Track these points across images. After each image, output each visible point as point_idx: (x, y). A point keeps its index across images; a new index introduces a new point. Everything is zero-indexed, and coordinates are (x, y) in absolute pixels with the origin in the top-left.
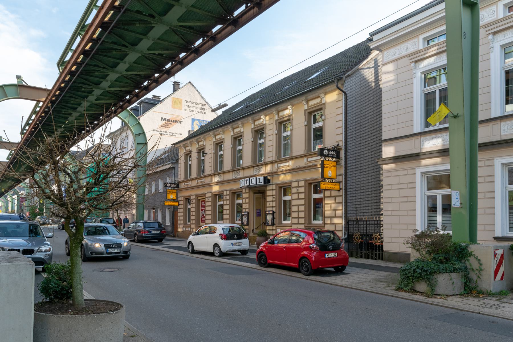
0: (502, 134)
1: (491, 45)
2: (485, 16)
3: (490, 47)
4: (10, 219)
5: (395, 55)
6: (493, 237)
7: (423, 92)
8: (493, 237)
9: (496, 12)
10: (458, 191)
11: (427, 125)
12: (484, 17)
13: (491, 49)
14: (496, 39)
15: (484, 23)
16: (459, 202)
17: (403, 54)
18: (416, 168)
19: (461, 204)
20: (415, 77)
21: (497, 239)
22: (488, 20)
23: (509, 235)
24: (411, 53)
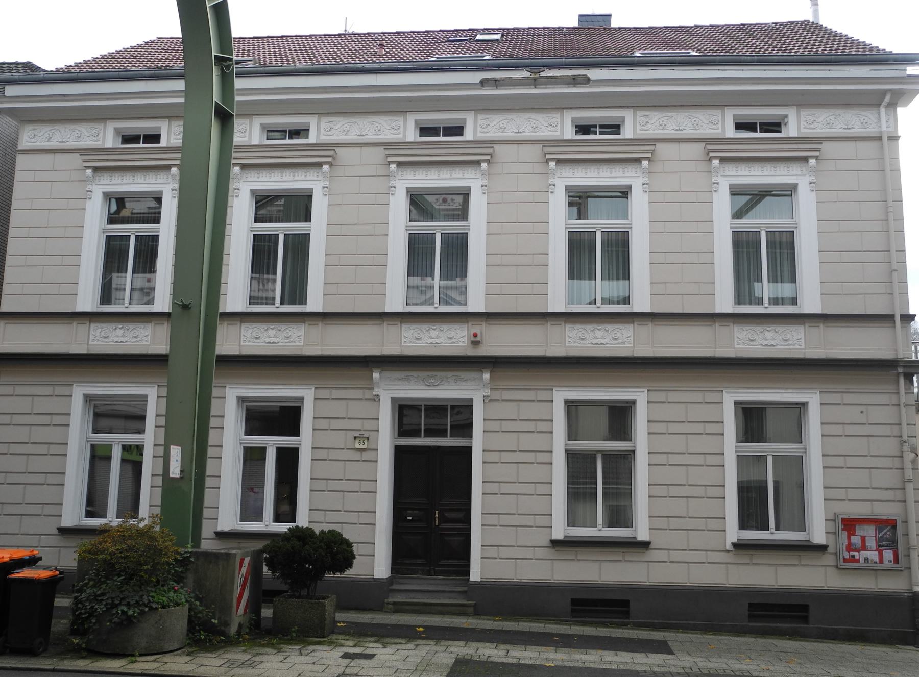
0: (91, 343)
1: (236, 184)
2: (83, 134)
3: (713, 181)
4: (544, 315)
5: (51, 140)
6: (58, 529)
7: (251, 231)
8: (58, 529)
9: (248, 130)
10: (179, 446)
11: (106, 295)
12: (82, 137)
13: (236, 191)
14: (97, 180)
15: (71, 145)
16: (179, 469)
17: (68, 143)
18: (74, 385)
19: (182, 471)
20: (90, 199)
21: (63, 531)
22: (388, 137)
23: (84, 524)
24: (71, 148)
